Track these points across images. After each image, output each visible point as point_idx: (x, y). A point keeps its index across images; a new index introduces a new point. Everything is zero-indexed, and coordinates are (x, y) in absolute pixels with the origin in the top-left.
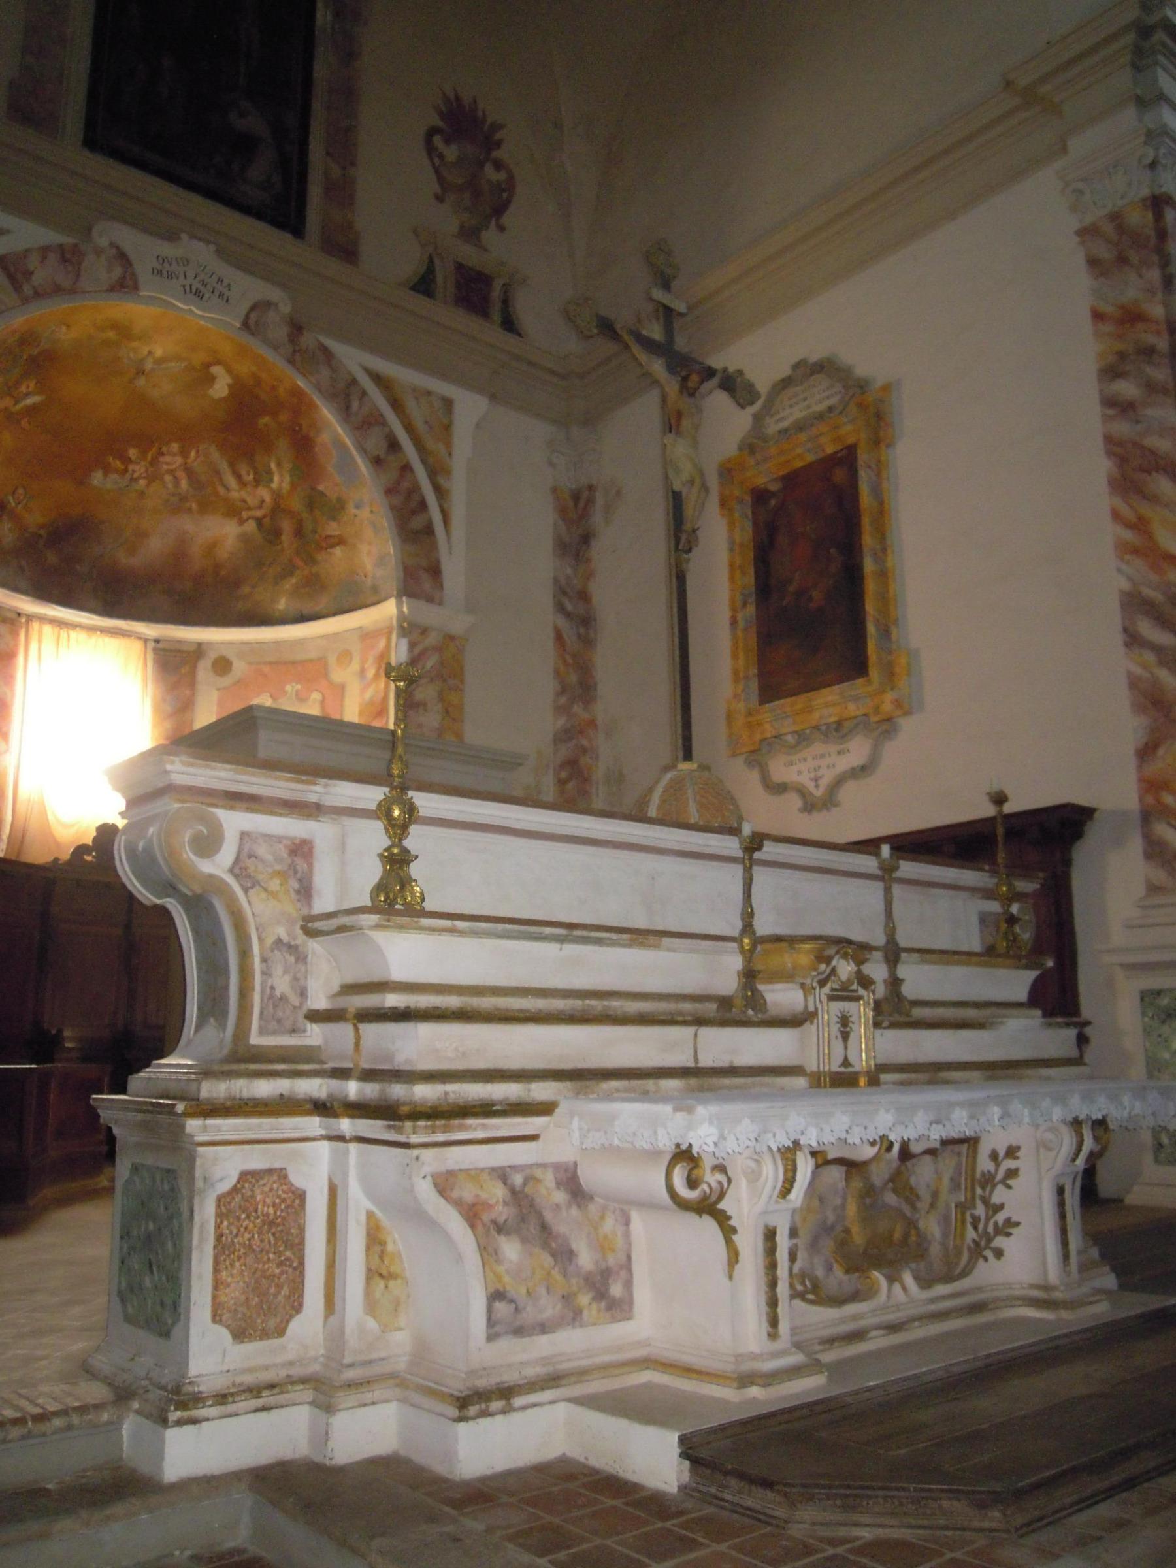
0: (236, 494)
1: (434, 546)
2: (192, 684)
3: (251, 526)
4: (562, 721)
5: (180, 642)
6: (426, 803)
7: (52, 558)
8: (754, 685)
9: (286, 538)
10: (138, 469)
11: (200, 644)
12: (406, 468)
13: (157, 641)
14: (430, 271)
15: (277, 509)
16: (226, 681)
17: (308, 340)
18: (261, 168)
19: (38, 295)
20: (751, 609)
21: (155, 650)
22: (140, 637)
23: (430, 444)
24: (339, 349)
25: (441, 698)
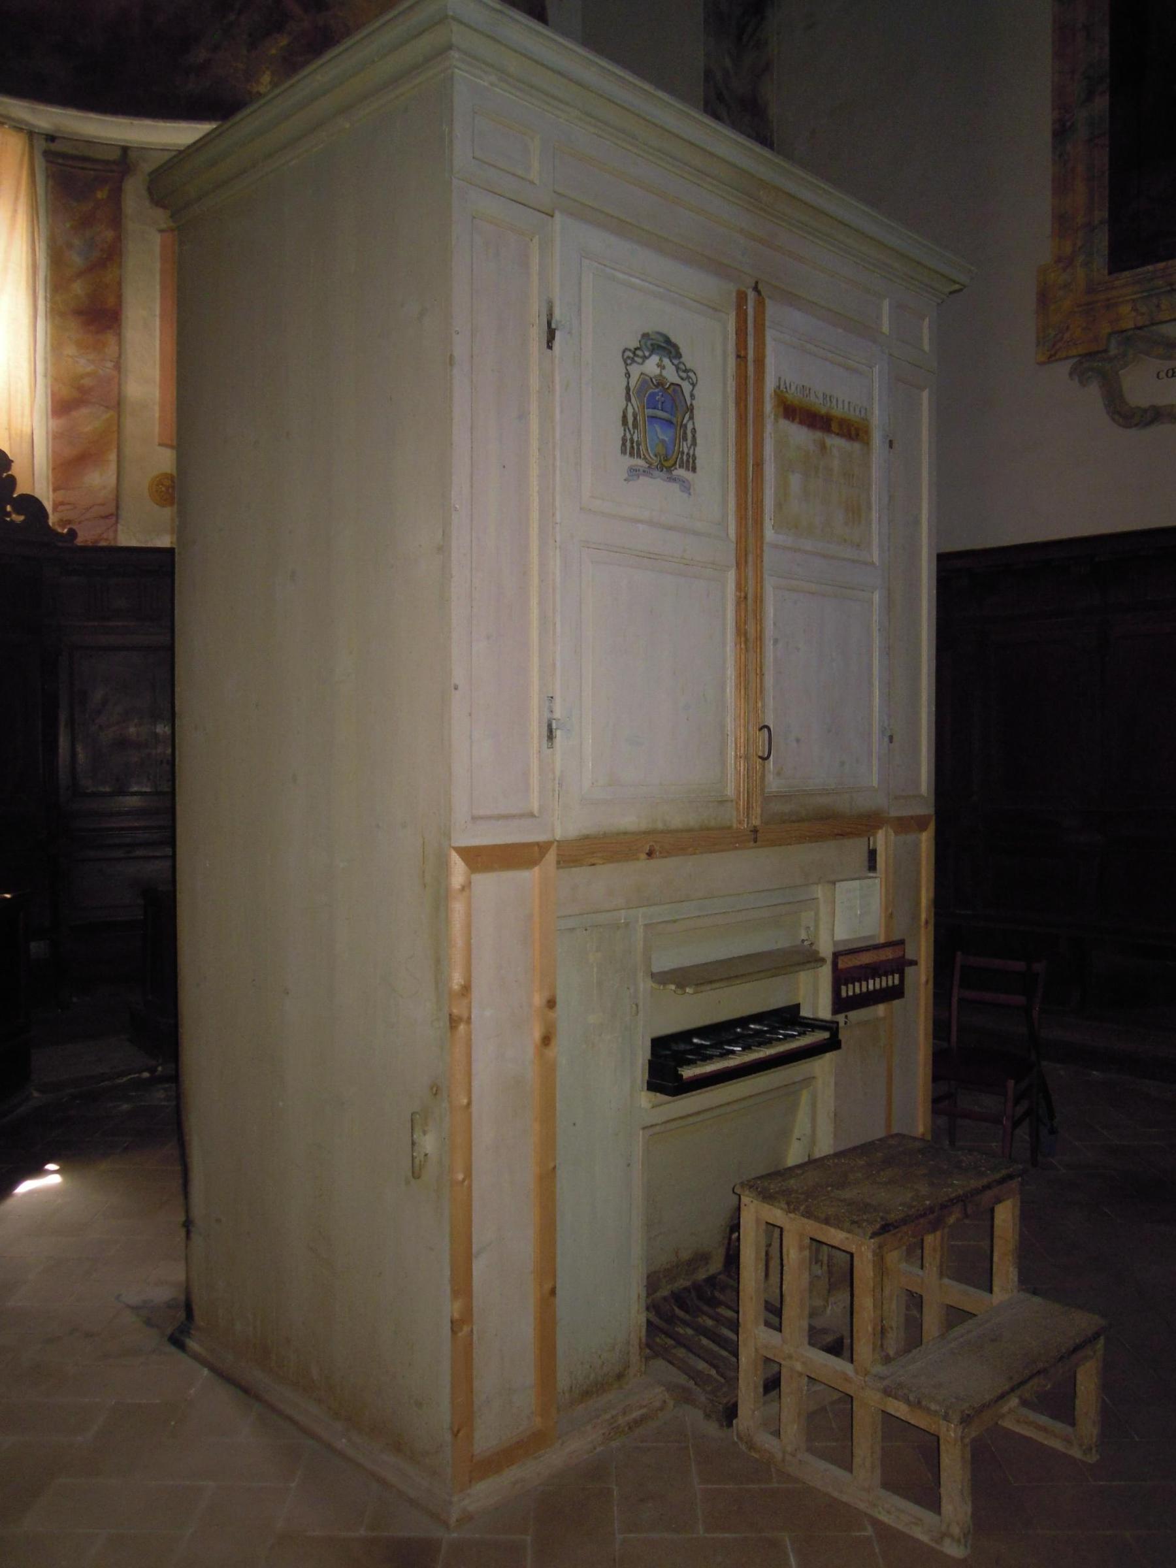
2: (117, 221)
5: (89, 143)
8: (1102, 240)
11: (125, 150)
13: (51, 138)
20: (1102, 103)
21: (46, 153)
22: (19, 127)
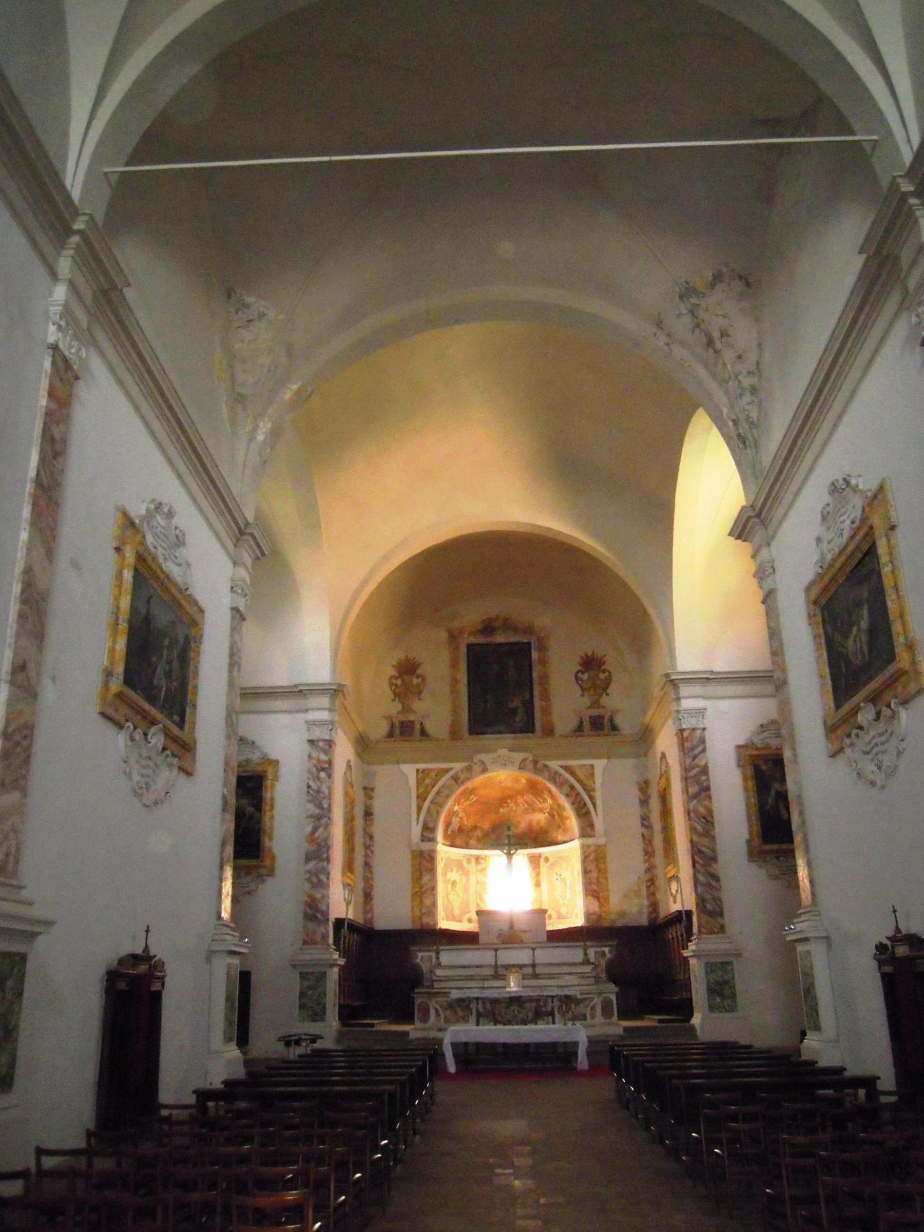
0: (540, 806)
1: (590, 817)
3: (547, 814)
4: (647, 865)
6: (441, 947)
7: (494, 836)
9: (557, 817)
10: (511, 805)
12: (578, 794)
14: (581, 723)
15: (552, 809)
16: (549, 864)
17: (540, 765)
18: (520, 717)
19: (462, 783)
23: (586, 782)
24: (551, 763)
25: (597, 867)
